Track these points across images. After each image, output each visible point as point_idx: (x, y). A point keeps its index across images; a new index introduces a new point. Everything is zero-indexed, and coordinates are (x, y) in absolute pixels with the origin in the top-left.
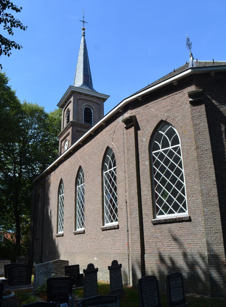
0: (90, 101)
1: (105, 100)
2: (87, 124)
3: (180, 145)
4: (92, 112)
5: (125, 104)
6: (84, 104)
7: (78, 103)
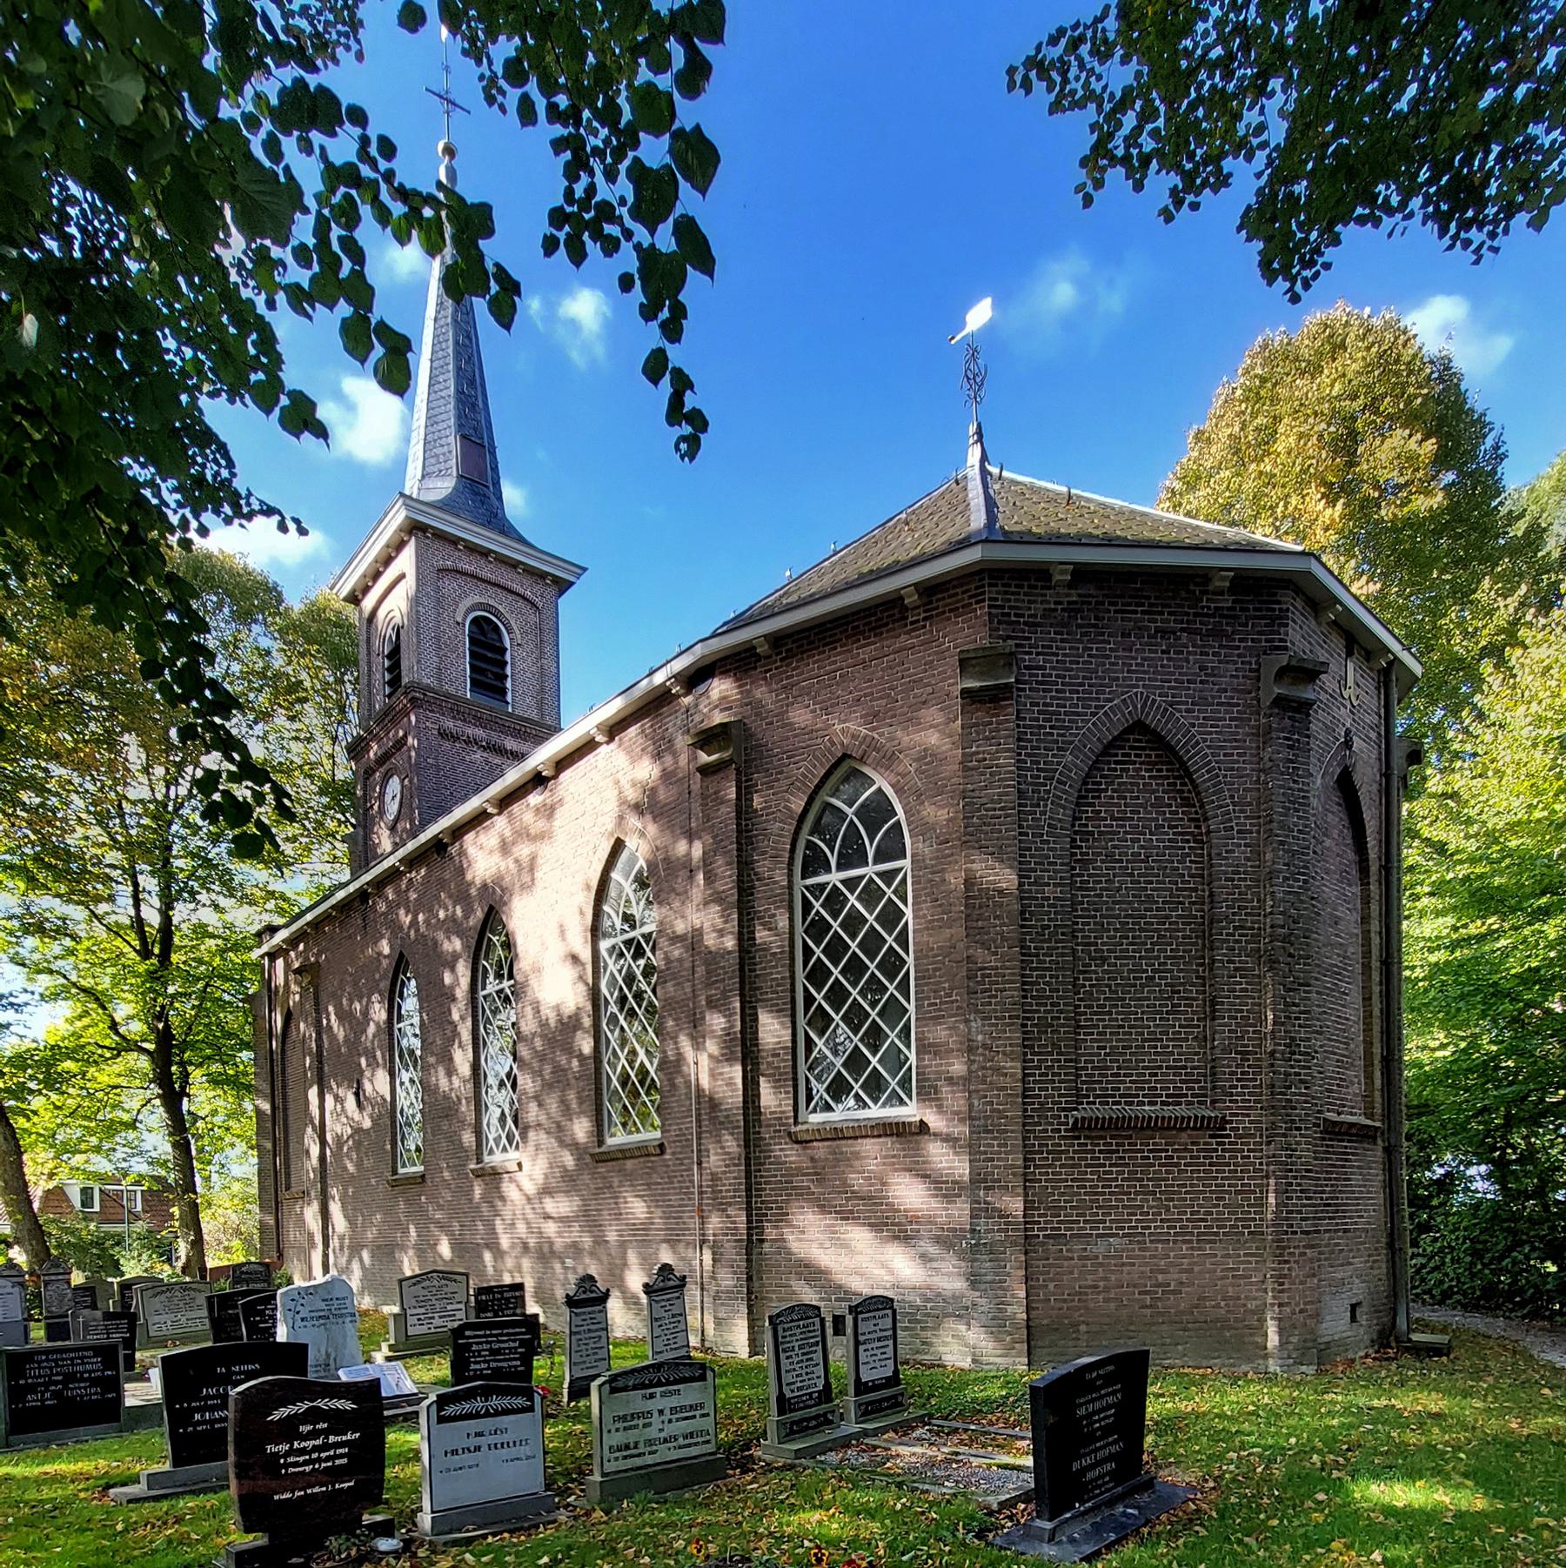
0: (489, 583)
1: (563, 586)
2: (483, 700)
3: (906, 863)
4: (508, 645)
5: (701, 664)
6: (468, 602)
7: (438, 590)
